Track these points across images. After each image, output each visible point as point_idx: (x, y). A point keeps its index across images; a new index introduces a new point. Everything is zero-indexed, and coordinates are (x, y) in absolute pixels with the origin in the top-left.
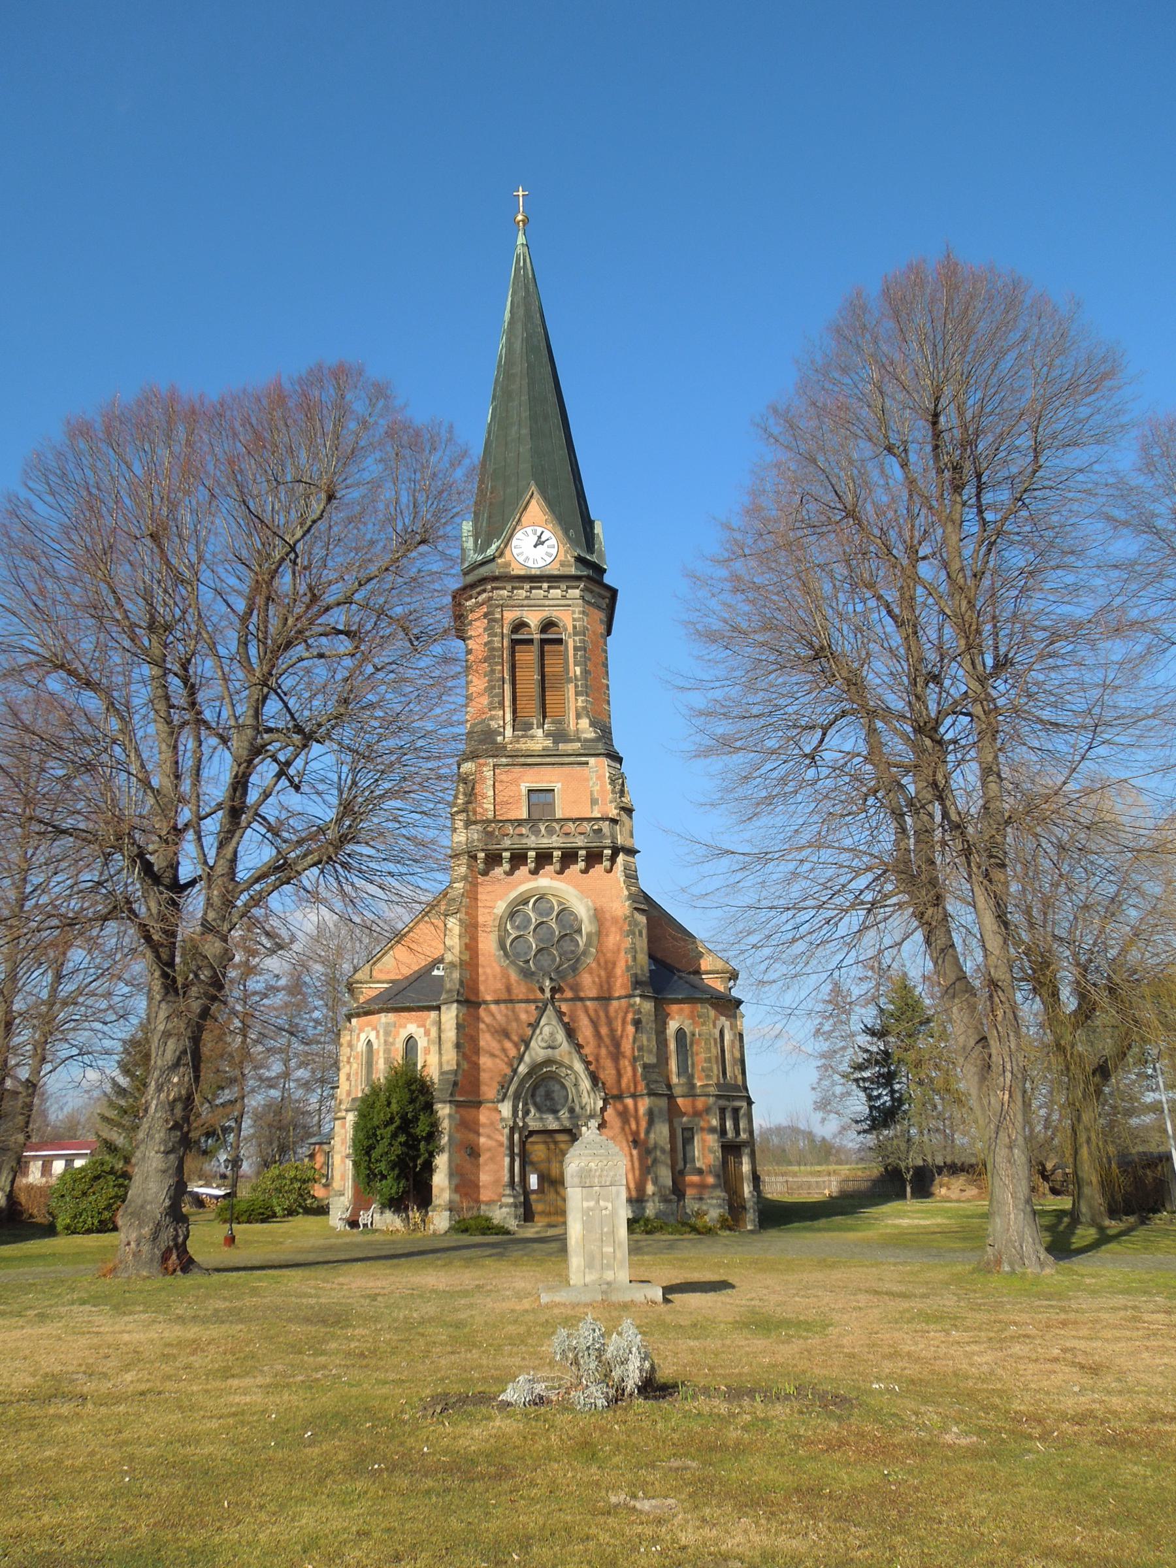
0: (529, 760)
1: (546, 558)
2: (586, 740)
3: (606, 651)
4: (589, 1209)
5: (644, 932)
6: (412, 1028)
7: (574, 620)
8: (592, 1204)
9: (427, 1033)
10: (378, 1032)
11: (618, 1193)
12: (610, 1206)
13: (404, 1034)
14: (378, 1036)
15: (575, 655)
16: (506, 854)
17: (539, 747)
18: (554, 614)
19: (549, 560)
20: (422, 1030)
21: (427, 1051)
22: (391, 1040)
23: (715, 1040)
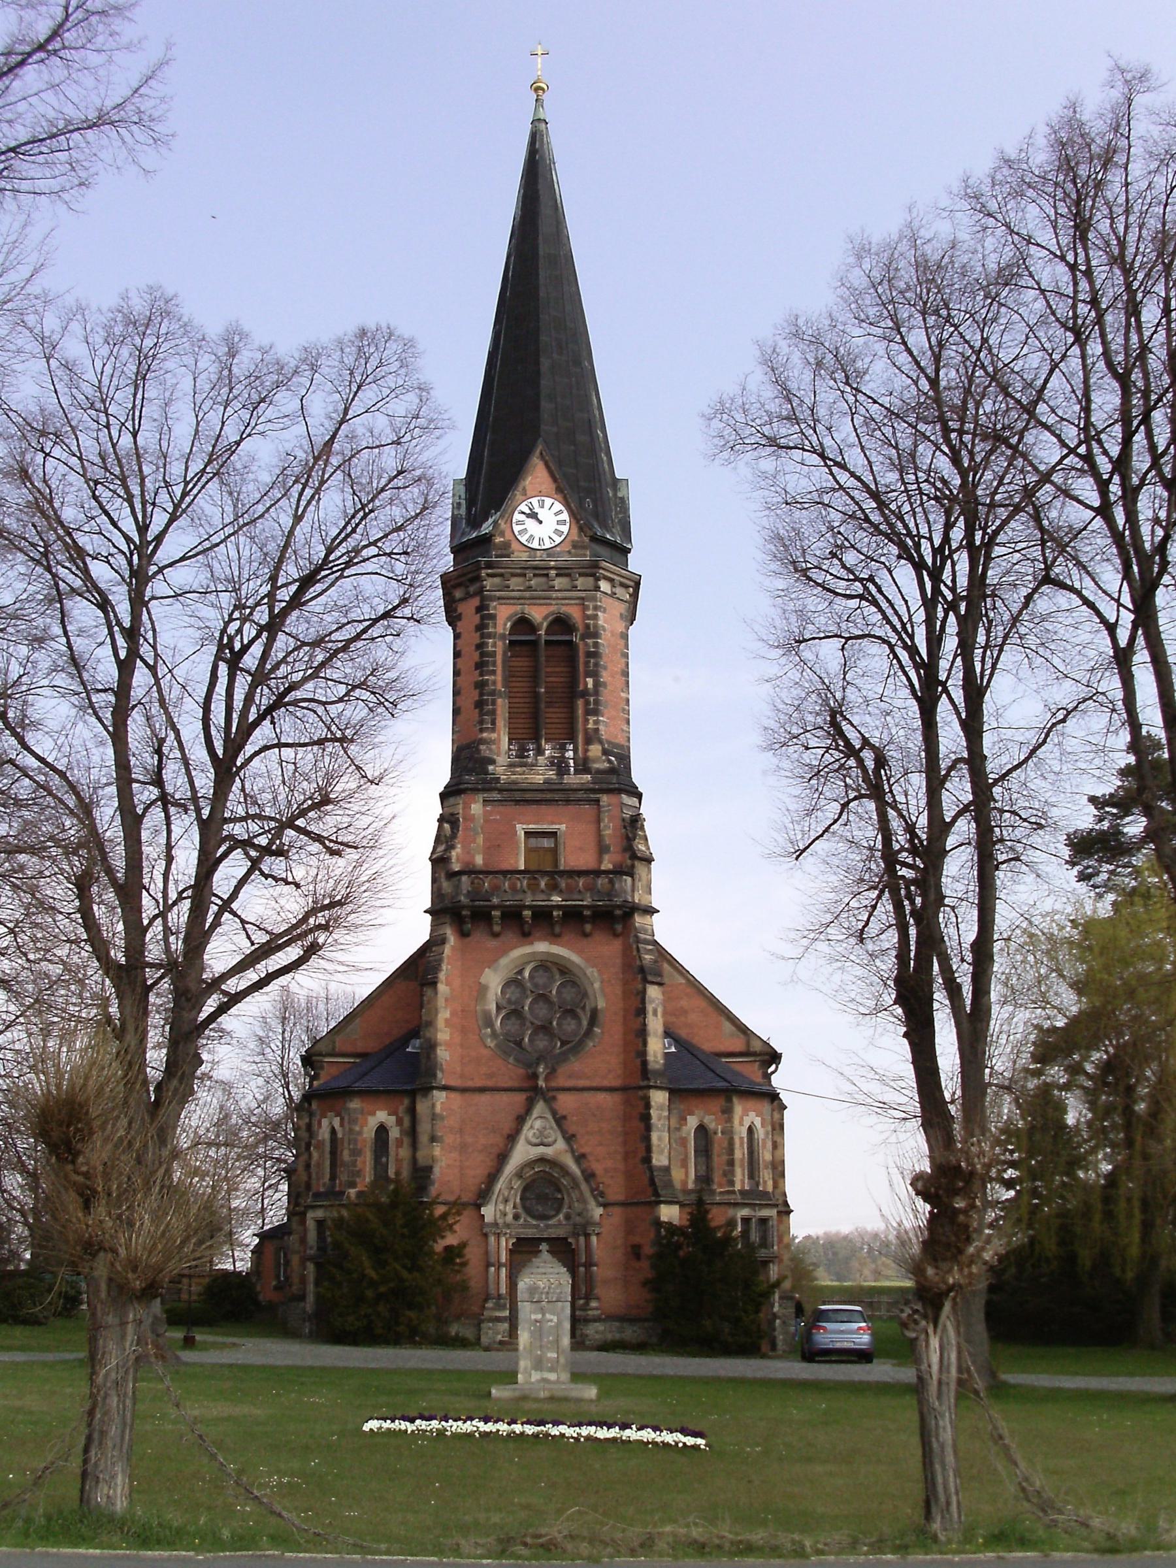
0: (528, 796)
1: (555, 537)
2: (599, 772)
3: (626, 656)
4: (536, 1321)
5: (660, 1010)
6: (382, 1116)
7: (588, 617)
8: (539, 1316)
9: (399, 1122)
10: (342, 1120)
11: (563, 1308)
12: (555, 1319)
13: (373, 1122)
14: (342, 1125)
15: (587, 663)
16: (496, 913)
17: (539, 779)
18: (564, 609)
19: (558, 540)
20: (393, 1118)
21: (399, 1143)
22: (357, 1128)
23: (741, 1138)
